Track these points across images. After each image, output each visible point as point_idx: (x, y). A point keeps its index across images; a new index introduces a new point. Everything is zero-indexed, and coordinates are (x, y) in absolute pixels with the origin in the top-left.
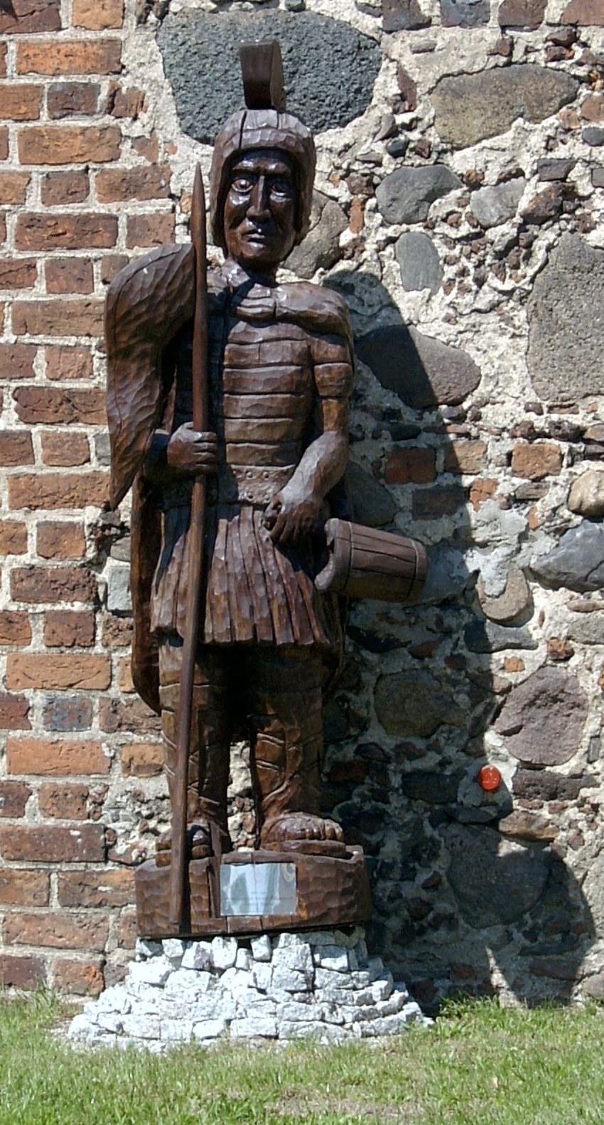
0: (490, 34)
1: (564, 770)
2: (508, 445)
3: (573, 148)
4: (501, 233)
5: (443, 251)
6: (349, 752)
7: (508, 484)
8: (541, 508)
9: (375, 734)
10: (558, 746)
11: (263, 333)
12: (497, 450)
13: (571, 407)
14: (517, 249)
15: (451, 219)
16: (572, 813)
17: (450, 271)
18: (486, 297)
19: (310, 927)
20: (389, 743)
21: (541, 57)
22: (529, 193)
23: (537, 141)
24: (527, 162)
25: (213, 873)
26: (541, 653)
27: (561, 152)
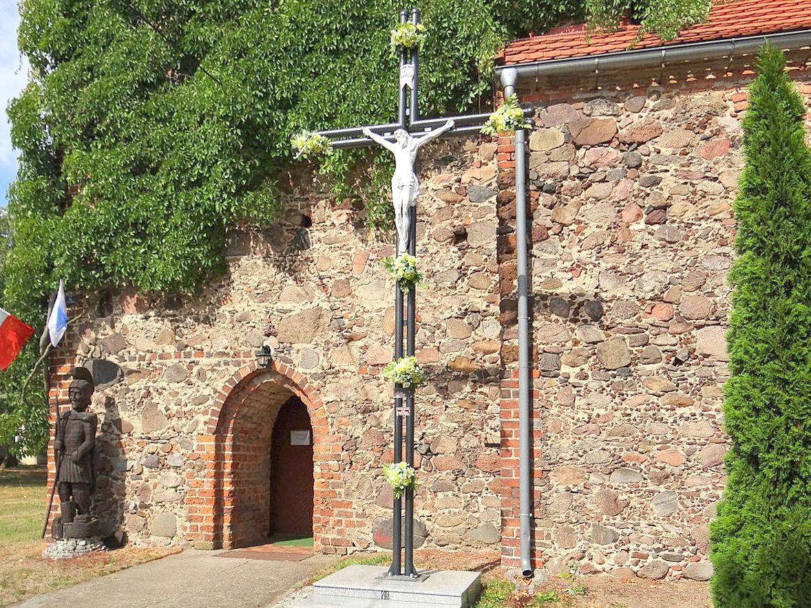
0: (137, 362)
1: (147, 503)
2: (138, 441)
3: (150, 384)
4: (138, 401)
5: (128, 404)
6: (111, 499)
7: (138, 448)
8: (144, 453)
9: (115, 496)
10: (147, 497)
11: (74, 422)
12: (136, 442)
13: (149, 433)
14: (141, 403)
15: (129, 398)
16: (149, 511)
17: (129, 408)
18: (135, 412)
19: (712, 62)
20: (118, 498)
21: (145, 367)
22: (143, 392)
23: (144, 383)
24: (142, 387)
25: (527, 245)
26: (143, 481)
27: (148, 385)
